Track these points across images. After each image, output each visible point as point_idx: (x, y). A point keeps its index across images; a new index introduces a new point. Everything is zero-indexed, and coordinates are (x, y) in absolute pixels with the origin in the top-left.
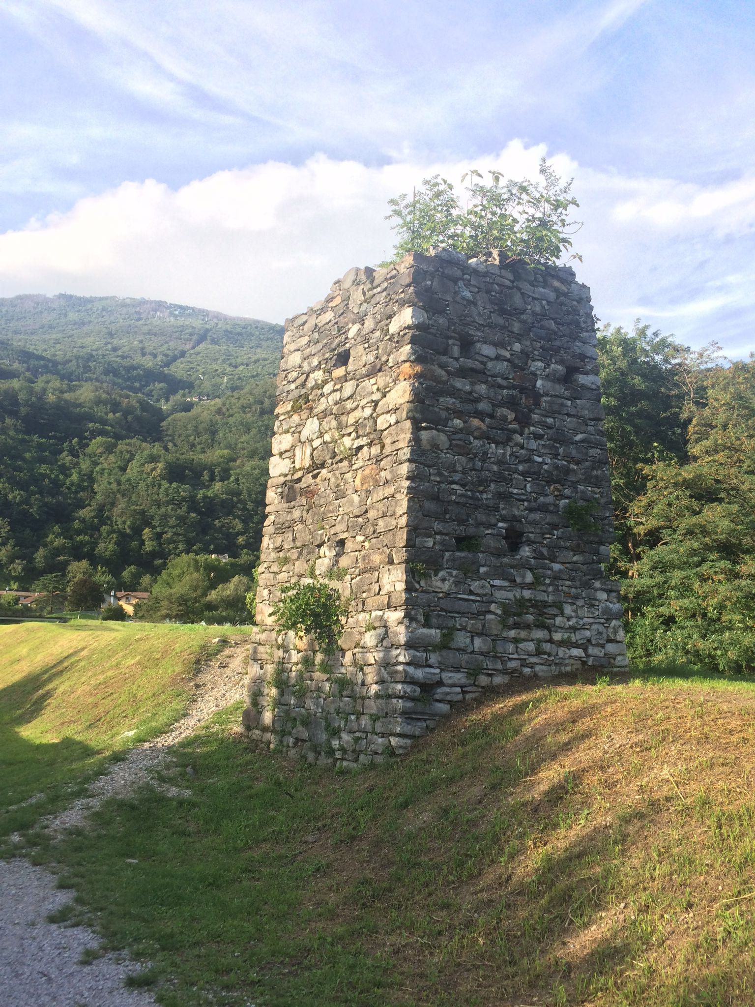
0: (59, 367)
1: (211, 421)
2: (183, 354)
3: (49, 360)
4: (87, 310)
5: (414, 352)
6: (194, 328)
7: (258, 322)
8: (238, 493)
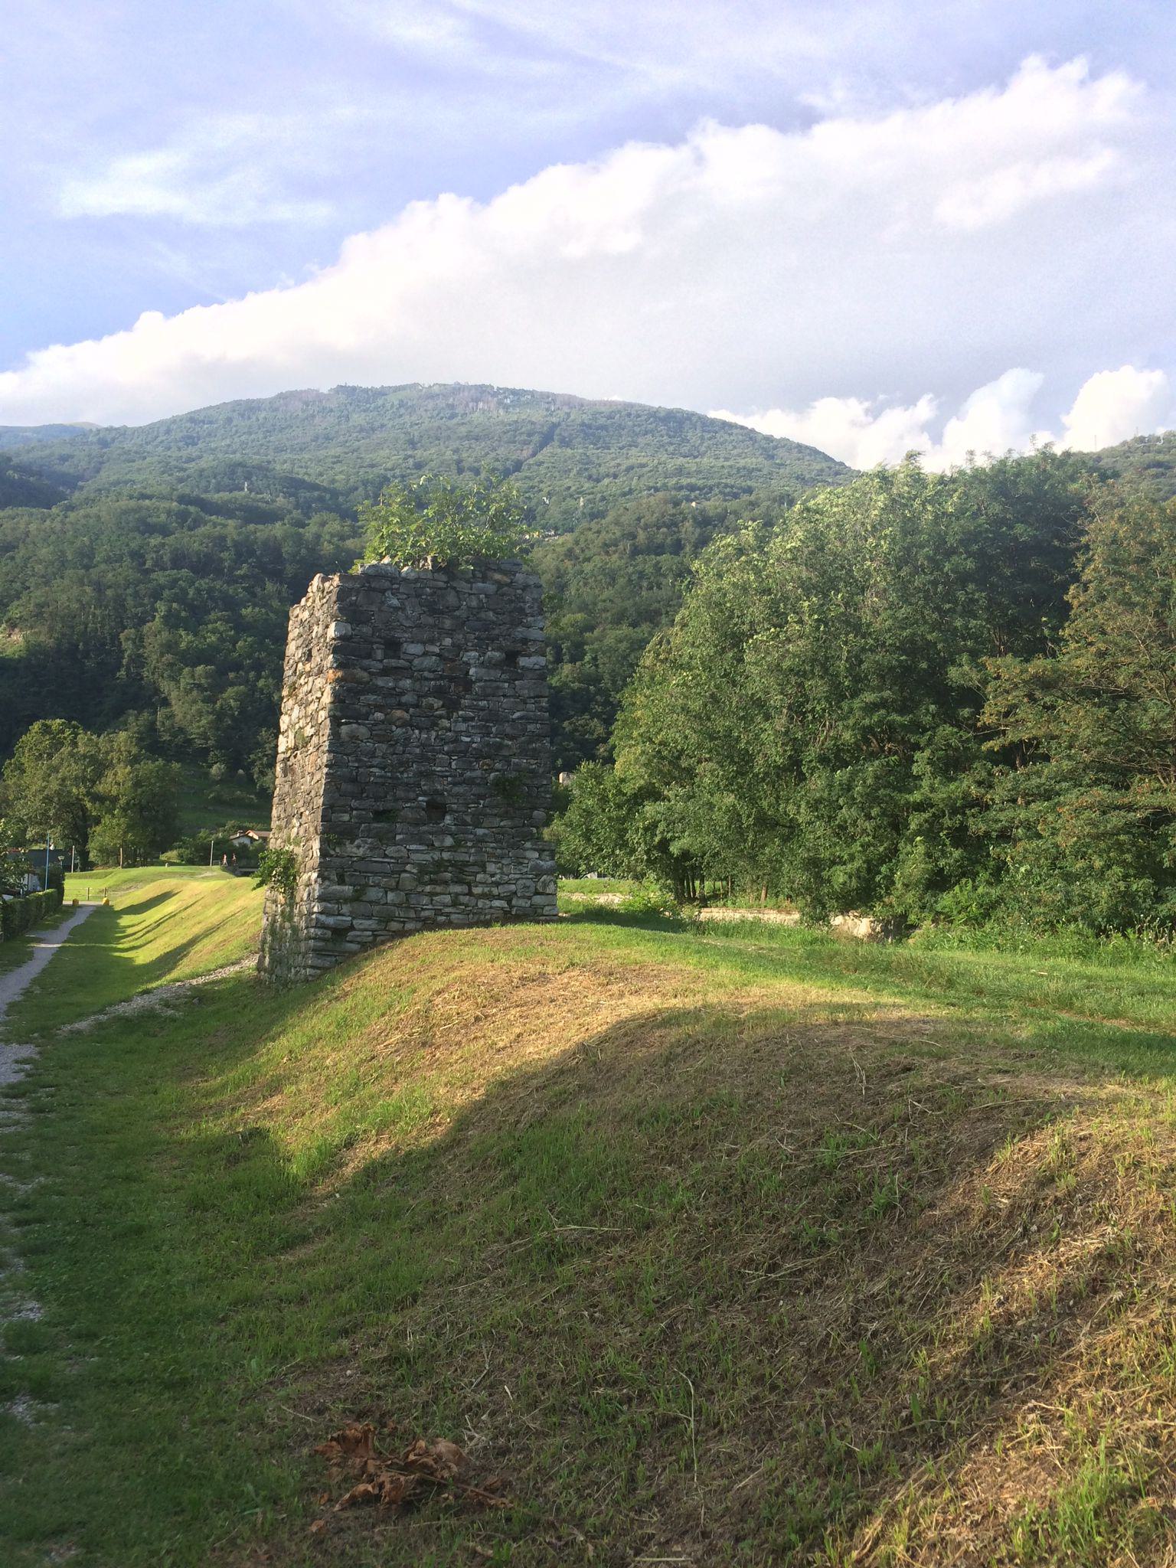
0: (341, 499)
1: (558, 569)
2: (518, 466)
3: (325, 490)
4: (376, 408)
5: (336, 660)
6: (533, 423)
7: (632, 405)
8: (596, 680)
